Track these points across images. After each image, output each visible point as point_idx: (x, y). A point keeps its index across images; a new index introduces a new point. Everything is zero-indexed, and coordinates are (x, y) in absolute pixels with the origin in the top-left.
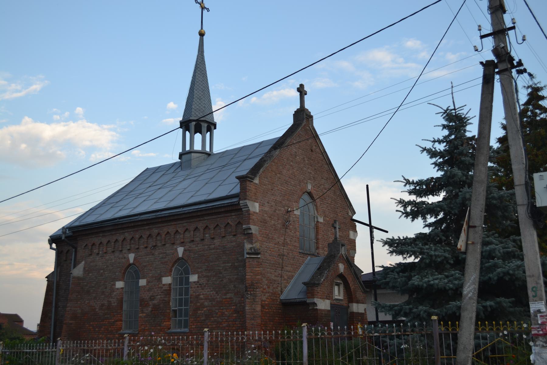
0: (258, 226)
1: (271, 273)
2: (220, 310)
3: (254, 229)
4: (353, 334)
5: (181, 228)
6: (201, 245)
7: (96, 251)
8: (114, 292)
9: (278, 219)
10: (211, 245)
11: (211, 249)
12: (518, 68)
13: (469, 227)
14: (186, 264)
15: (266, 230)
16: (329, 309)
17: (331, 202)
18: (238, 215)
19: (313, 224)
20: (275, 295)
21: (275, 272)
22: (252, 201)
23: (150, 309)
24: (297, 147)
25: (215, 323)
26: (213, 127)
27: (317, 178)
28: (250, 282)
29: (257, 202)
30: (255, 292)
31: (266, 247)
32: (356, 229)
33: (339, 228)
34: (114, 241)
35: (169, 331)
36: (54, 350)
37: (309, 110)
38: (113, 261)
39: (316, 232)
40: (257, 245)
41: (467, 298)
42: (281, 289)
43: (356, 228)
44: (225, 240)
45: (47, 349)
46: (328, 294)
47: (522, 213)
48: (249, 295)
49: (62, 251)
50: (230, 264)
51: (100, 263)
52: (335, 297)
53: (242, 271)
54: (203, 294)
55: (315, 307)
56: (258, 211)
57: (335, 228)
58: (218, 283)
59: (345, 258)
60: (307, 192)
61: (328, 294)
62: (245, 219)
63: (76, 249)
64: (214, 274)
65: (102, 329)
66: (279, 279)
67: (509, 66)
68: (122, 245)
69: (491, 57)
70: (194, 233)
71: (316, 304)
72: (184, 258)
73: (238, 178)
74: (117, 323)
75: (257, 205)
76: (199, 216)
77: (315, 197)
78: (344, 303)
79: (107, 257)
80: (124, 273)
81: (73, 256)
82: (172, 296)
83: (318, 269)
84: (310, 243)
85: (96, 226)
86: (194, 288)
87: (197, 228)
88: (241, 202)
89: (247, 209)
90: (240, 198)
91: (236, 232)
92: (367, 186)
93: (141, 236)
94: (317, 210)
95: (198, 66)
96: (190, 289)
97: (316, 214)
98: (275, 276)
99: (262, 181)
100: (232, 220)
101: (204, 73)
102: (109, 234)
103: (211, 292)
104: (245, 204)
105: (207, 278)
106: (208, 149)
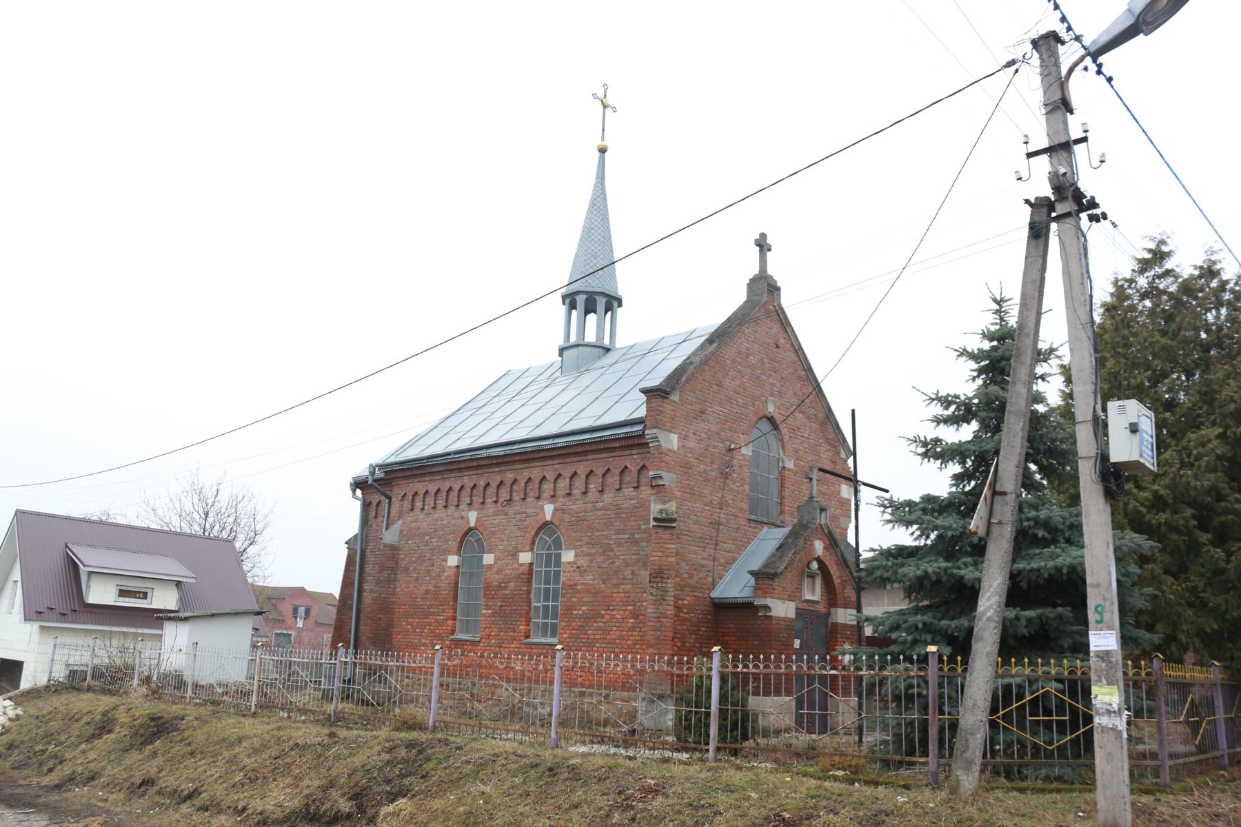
0: (674, 473)
1: (696, 553)
2: (608, 612)
3: (668, 478)
4: (794, 669)
6: (582, 502)
7: (419, 504)
8: (444, 571)
10: (597, 502)
11: (598, 510)
12: (1090, 212)
13: (995, 493)
14: (556, 533)
15: (689, 480)
16: (793, 616)
17: (810, 435)
19: (776, 472)
20: (703, 590)
21: (703, 551)
22: (666, 430)
25: (600, 632)
26: (615, 304)
30: (664, 585)
31: (688, 509)
34: (447, 489)
35: (527, 640)
36: (333, 661)
37: (775, 278)
38: (445, 522)
40: (672, 507)
41: (985, 619)
46: (793, 592)
47: (1087, 473)
49: (370, 503)
50: (627, 536)
56: (675, 447)
57: (811, 479)
59: (826, 531)
60: (767, 418)
61: (793, 592)
62: (653, 462)
63: (390, 498)
64: (601, 551)
65: (426, 631)
66: (710, 563)
67: (1076, 208)
69: (1047, 192)
70: (571, 481)
71: (769, 608)
72: (554, 522)
73: (644, 391)
75: (674, 437)
78: (822, 608)
79: (436, 516)
80: (461, 543)
81: (386, 511)
83: (777, 549)
86: (569, 572)
88: (647, 432)
91: (638, 482)
92: (853, 411)
94: (783, 447)
97: (781, 454)
98: (703, 558)
99: (685, 396)
100: (632, 461)
102: (439, 477)
104: (654, 435)
106: (607, 342)
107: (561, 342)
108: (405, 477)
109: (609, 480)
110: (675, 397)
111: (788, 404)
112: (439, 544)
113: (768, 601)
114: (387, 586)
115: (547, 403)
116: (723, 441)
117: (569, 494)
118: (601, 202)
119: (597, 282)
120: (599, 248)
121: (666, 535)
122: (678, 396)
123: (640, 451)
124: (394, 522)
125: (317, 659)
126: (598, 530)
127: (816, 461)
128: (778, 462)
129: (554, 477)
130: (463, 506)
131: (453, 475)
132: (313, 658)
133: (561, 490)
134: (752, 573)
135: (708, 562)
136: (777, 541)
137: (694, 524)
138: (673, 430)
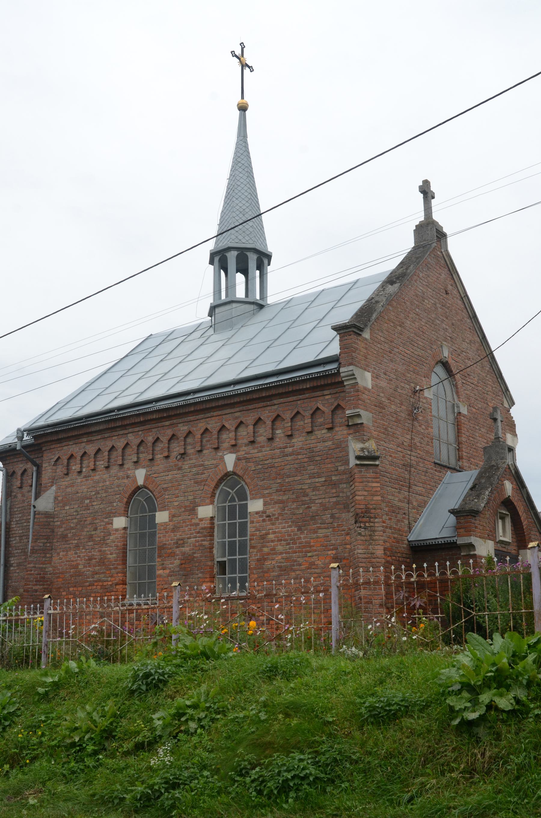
0: (371, 412)
1: (393, 495)
3: (366, 417)
5: (230, 422)
6: (268, 449)
7: (75, 467)
8: (110, 535)
9: (402, 404)
10: (286, 447)
11: (287, 455)
14: (240, 483)
18: (336, 393)
21: (399, 493)
22: (361, 368)
23: (177, 562)
24: (424, 283)
26: (266, 261)
27: (456, 340)
28: (362, 507)
29: (368, 372)
30: (372, 524)
32: (515, 432)
33: (502, 421)
34: (108, 448)
38: (108, 483)
39: (456, 431)
40: (372, 445)
42: (409, 522)
43: (515, 429)
44: (312, 438)
45: (24, 615)
48: (363, 530)
49: (14, 472)
50: (323, 479)
51: (84, 487)
52: (499, 538)
53: (345, 490)
54: (274, 533)
55: (470, 551)
56: (370, 386)
57: (495, 420)
58: (301, 512)
59: (513, 472)
62: (350, 400)
63: (39, 468)
64: (294, 496)
68: (123, 456)
70: (254, 428)
72: (237, 472)
74: (117, 587)
75: (368, 375)
76: (263, 397)
77: (455, 371)
79: (97, 477)
80: (128, 503)
82: (217, 539)
84: (448, 449)
85: (76, 424)
86: (258, 522)
87: (260, 419)
88: (342, 370)
89: (353, 382)
90: (340, 364)
91: (332, 422)
93: (158, 439)
94: (457, 393)
95: (245, 154)
96: (249, 525)
97: (456, 400)
98: (400, 501)
99: (375, 335)
101: (249, 171)
102: (99, 437)
103: (290, 529)
104: (350, 373)
105: (281, 505)
107: (210, 300)
108: (58, 440)
109: (299, 423)
110: (366, 335)
111: (459, 351)
112: (102, 506)
113: (473, 540)
114: (43, 555)
115: (209, 357)
116: (409, 383)
117: (253, 442)
118: (245, 159)
119: (247, 238)
120: (247, 205)
121: (370, 474)
122: (369, 334)
123: (332, 391)
124: (47, 489)
125: (17, 615)
126: (288, 476)
127: (485, 409)
128: (454, 408)
129: (235, 426)
130: (129, 465)
131: (115, 433)
132: (11, 615)
133: (243, 439)
134: (452, 512)
135: (403, 504)
136: (464, 484)
137: (391, 465)
138: (367, 368)
